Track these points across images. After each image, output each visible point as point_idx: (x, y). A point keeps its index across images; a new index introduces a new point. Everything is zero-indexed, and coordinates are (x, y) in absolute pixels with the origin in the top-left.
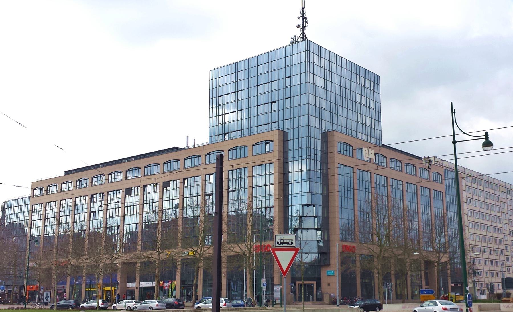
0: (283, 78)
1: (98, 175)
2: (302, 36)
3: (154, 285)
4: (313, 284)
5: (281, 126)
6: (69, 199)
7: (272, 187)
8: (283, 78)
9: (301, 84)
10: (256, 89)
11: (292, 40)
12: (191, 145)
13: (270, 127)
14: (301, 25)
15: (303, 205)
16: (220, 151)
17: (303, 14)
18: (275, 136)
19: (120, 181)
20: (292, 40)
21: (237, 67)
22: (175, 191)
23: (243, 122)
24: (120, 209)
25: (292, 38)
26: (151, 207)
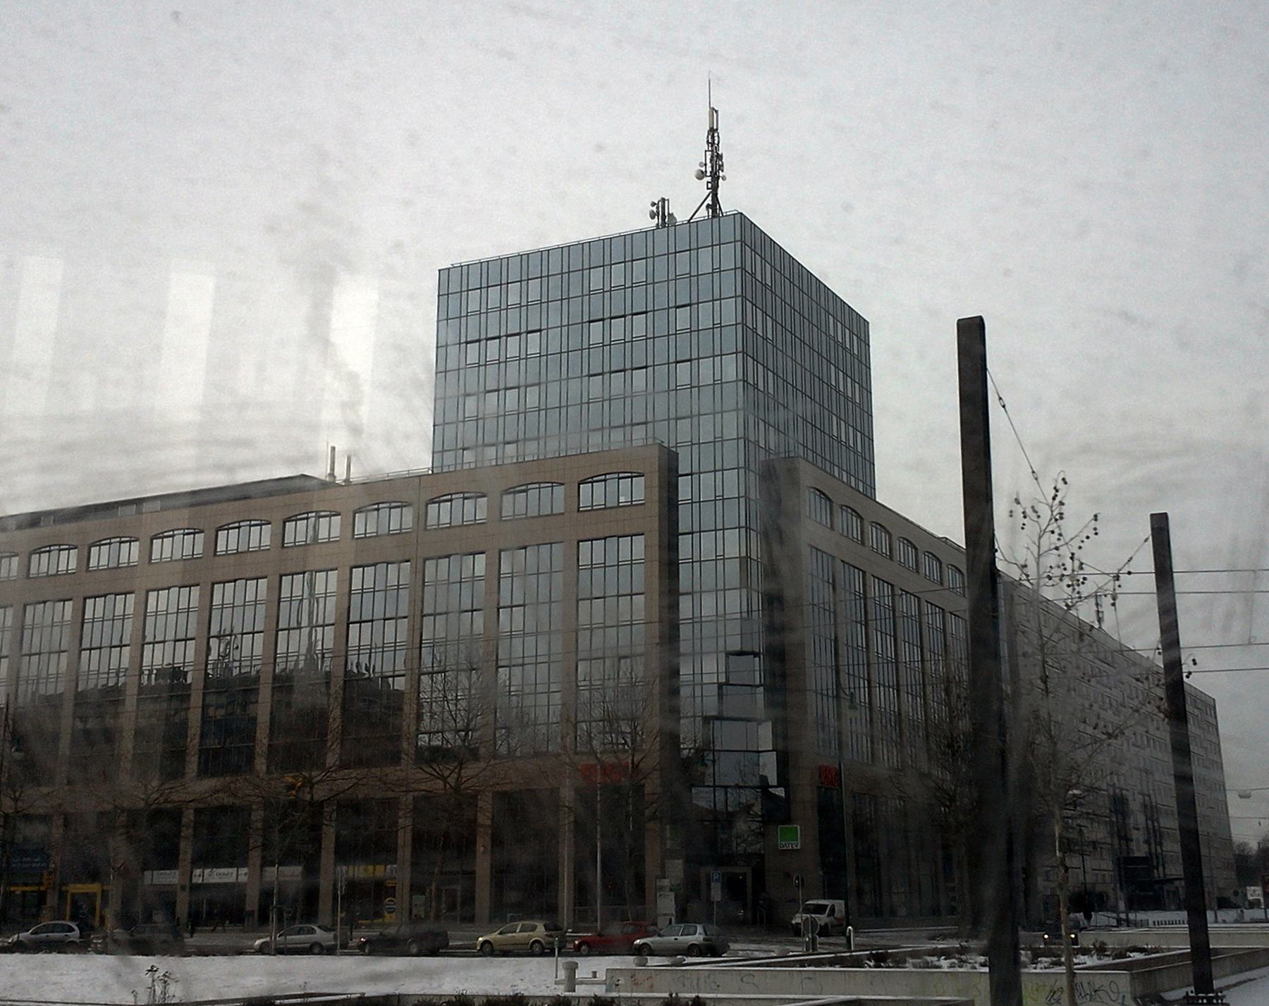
0: (669, 308)
1: (307, 513)
2: (709, 201)
3: (243, 879)
4: (744, 875)
5: (662, 435)
6: (40, 603)
7: (639, 600)
8: (669, 308)
9: (721, 327)
10: (586, 330)
11: (654, 209)
12: (341, 474)
13: (500, 454)
14: (708, 174)
15: (728, 654)
16: (259, 522)
17: (713, 144)
18: (652, 463)
19: (329, 542)
20: (654, 209)
21: (565, 259)
22: (56, 630)
23: (501, 426)
24: (191, 644)
25: (653, 204)
26: (43, 666)
